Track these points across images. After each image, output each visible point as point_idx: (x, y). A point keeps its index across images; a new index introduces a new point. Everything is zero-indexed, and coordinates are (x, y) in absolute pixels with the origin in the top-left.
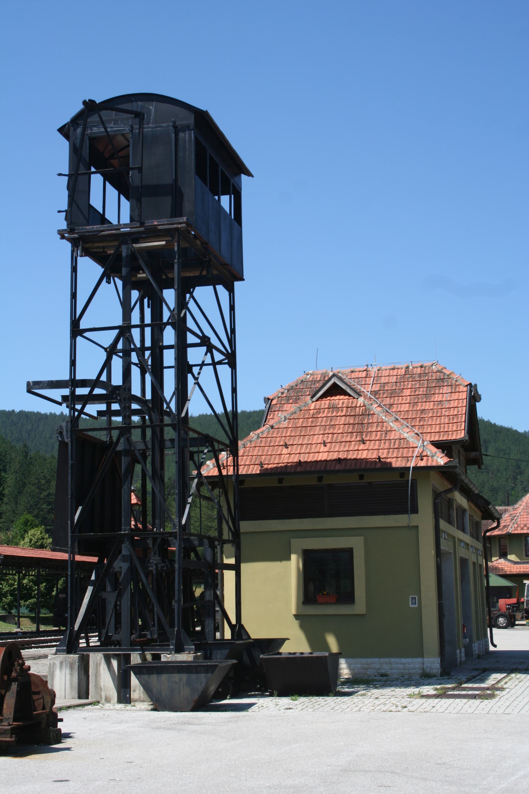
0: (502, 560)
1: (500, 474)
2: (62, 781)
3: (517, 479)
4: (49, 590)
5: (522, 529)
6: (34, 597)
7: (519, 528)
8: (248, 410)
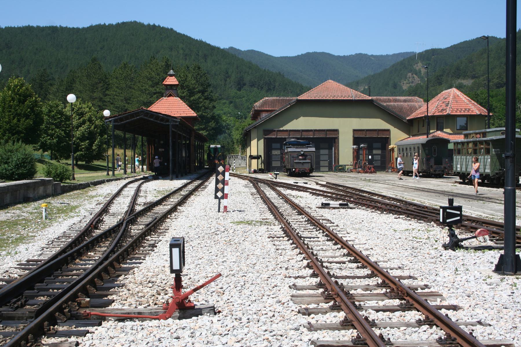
0: (439, 132)
1: (217, 77)
2: (329, 282)
3: (227, 80)
4: (91, 144)
5: (456, 112)
6: (81, 150)
7: (462, 111)
8: (42, 26)
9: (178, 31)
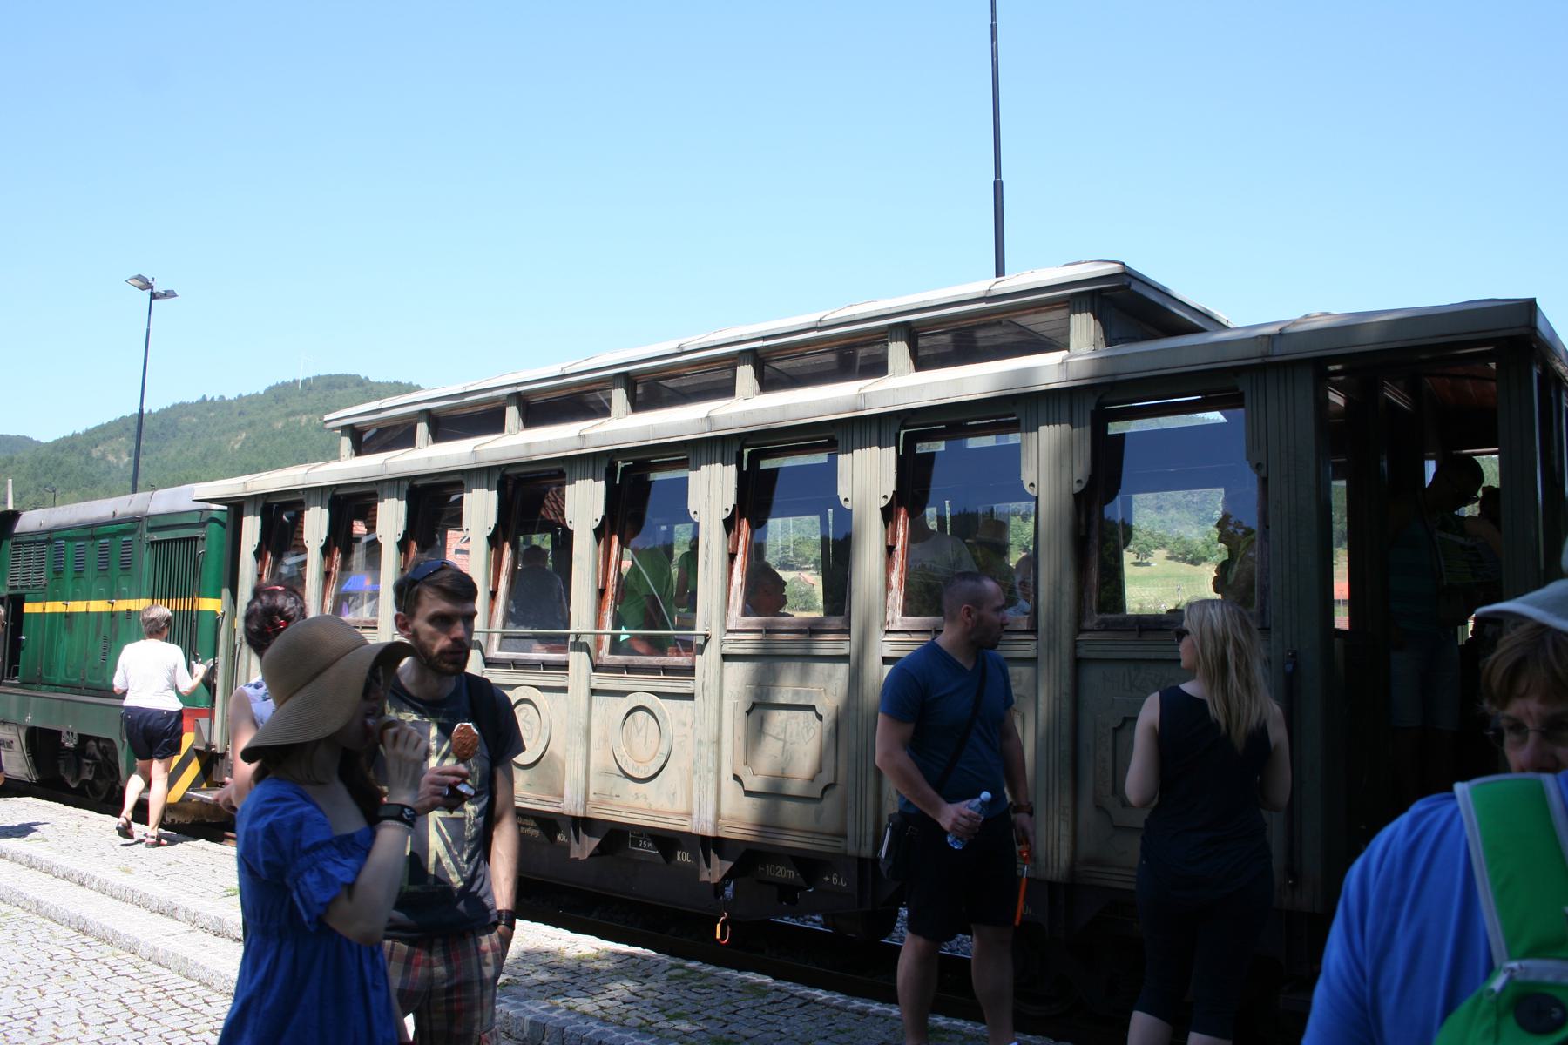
9: (231, 395)
